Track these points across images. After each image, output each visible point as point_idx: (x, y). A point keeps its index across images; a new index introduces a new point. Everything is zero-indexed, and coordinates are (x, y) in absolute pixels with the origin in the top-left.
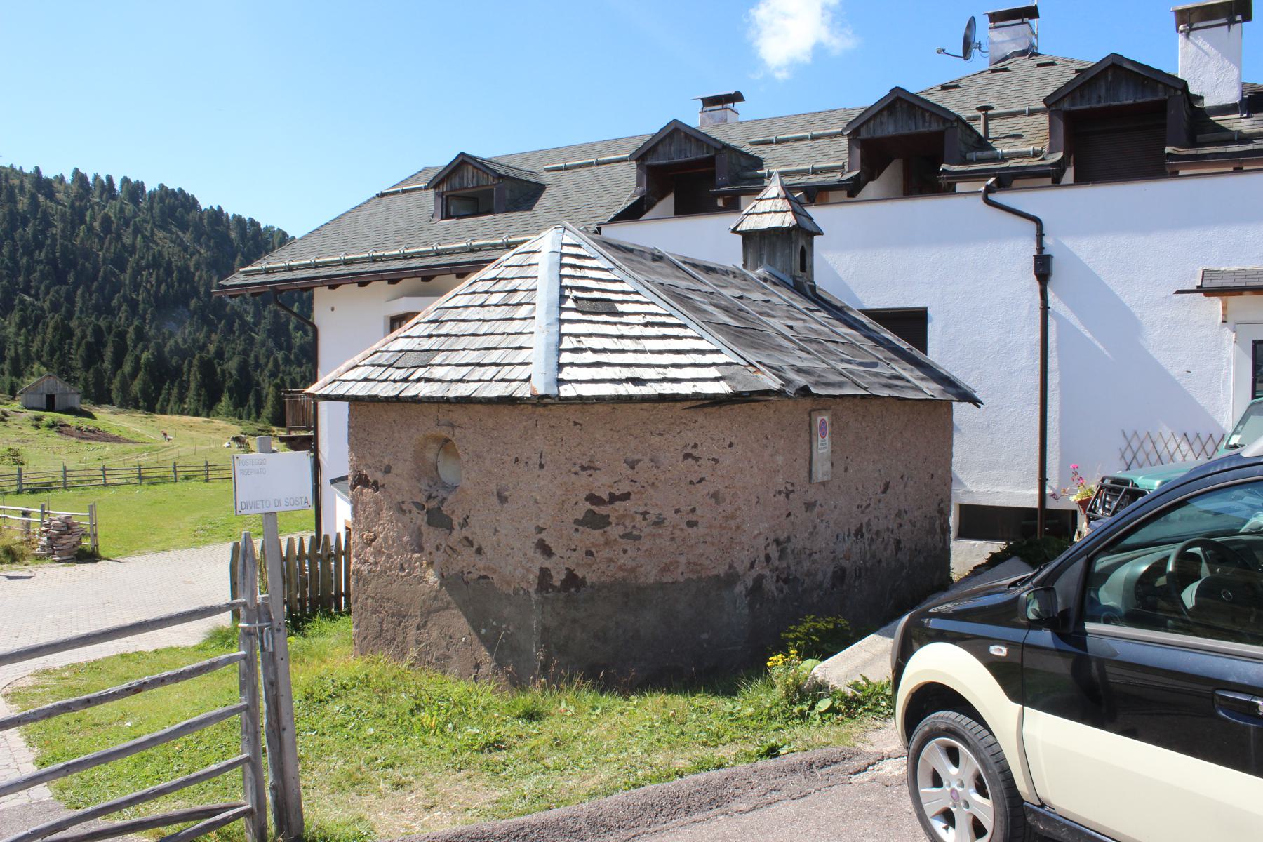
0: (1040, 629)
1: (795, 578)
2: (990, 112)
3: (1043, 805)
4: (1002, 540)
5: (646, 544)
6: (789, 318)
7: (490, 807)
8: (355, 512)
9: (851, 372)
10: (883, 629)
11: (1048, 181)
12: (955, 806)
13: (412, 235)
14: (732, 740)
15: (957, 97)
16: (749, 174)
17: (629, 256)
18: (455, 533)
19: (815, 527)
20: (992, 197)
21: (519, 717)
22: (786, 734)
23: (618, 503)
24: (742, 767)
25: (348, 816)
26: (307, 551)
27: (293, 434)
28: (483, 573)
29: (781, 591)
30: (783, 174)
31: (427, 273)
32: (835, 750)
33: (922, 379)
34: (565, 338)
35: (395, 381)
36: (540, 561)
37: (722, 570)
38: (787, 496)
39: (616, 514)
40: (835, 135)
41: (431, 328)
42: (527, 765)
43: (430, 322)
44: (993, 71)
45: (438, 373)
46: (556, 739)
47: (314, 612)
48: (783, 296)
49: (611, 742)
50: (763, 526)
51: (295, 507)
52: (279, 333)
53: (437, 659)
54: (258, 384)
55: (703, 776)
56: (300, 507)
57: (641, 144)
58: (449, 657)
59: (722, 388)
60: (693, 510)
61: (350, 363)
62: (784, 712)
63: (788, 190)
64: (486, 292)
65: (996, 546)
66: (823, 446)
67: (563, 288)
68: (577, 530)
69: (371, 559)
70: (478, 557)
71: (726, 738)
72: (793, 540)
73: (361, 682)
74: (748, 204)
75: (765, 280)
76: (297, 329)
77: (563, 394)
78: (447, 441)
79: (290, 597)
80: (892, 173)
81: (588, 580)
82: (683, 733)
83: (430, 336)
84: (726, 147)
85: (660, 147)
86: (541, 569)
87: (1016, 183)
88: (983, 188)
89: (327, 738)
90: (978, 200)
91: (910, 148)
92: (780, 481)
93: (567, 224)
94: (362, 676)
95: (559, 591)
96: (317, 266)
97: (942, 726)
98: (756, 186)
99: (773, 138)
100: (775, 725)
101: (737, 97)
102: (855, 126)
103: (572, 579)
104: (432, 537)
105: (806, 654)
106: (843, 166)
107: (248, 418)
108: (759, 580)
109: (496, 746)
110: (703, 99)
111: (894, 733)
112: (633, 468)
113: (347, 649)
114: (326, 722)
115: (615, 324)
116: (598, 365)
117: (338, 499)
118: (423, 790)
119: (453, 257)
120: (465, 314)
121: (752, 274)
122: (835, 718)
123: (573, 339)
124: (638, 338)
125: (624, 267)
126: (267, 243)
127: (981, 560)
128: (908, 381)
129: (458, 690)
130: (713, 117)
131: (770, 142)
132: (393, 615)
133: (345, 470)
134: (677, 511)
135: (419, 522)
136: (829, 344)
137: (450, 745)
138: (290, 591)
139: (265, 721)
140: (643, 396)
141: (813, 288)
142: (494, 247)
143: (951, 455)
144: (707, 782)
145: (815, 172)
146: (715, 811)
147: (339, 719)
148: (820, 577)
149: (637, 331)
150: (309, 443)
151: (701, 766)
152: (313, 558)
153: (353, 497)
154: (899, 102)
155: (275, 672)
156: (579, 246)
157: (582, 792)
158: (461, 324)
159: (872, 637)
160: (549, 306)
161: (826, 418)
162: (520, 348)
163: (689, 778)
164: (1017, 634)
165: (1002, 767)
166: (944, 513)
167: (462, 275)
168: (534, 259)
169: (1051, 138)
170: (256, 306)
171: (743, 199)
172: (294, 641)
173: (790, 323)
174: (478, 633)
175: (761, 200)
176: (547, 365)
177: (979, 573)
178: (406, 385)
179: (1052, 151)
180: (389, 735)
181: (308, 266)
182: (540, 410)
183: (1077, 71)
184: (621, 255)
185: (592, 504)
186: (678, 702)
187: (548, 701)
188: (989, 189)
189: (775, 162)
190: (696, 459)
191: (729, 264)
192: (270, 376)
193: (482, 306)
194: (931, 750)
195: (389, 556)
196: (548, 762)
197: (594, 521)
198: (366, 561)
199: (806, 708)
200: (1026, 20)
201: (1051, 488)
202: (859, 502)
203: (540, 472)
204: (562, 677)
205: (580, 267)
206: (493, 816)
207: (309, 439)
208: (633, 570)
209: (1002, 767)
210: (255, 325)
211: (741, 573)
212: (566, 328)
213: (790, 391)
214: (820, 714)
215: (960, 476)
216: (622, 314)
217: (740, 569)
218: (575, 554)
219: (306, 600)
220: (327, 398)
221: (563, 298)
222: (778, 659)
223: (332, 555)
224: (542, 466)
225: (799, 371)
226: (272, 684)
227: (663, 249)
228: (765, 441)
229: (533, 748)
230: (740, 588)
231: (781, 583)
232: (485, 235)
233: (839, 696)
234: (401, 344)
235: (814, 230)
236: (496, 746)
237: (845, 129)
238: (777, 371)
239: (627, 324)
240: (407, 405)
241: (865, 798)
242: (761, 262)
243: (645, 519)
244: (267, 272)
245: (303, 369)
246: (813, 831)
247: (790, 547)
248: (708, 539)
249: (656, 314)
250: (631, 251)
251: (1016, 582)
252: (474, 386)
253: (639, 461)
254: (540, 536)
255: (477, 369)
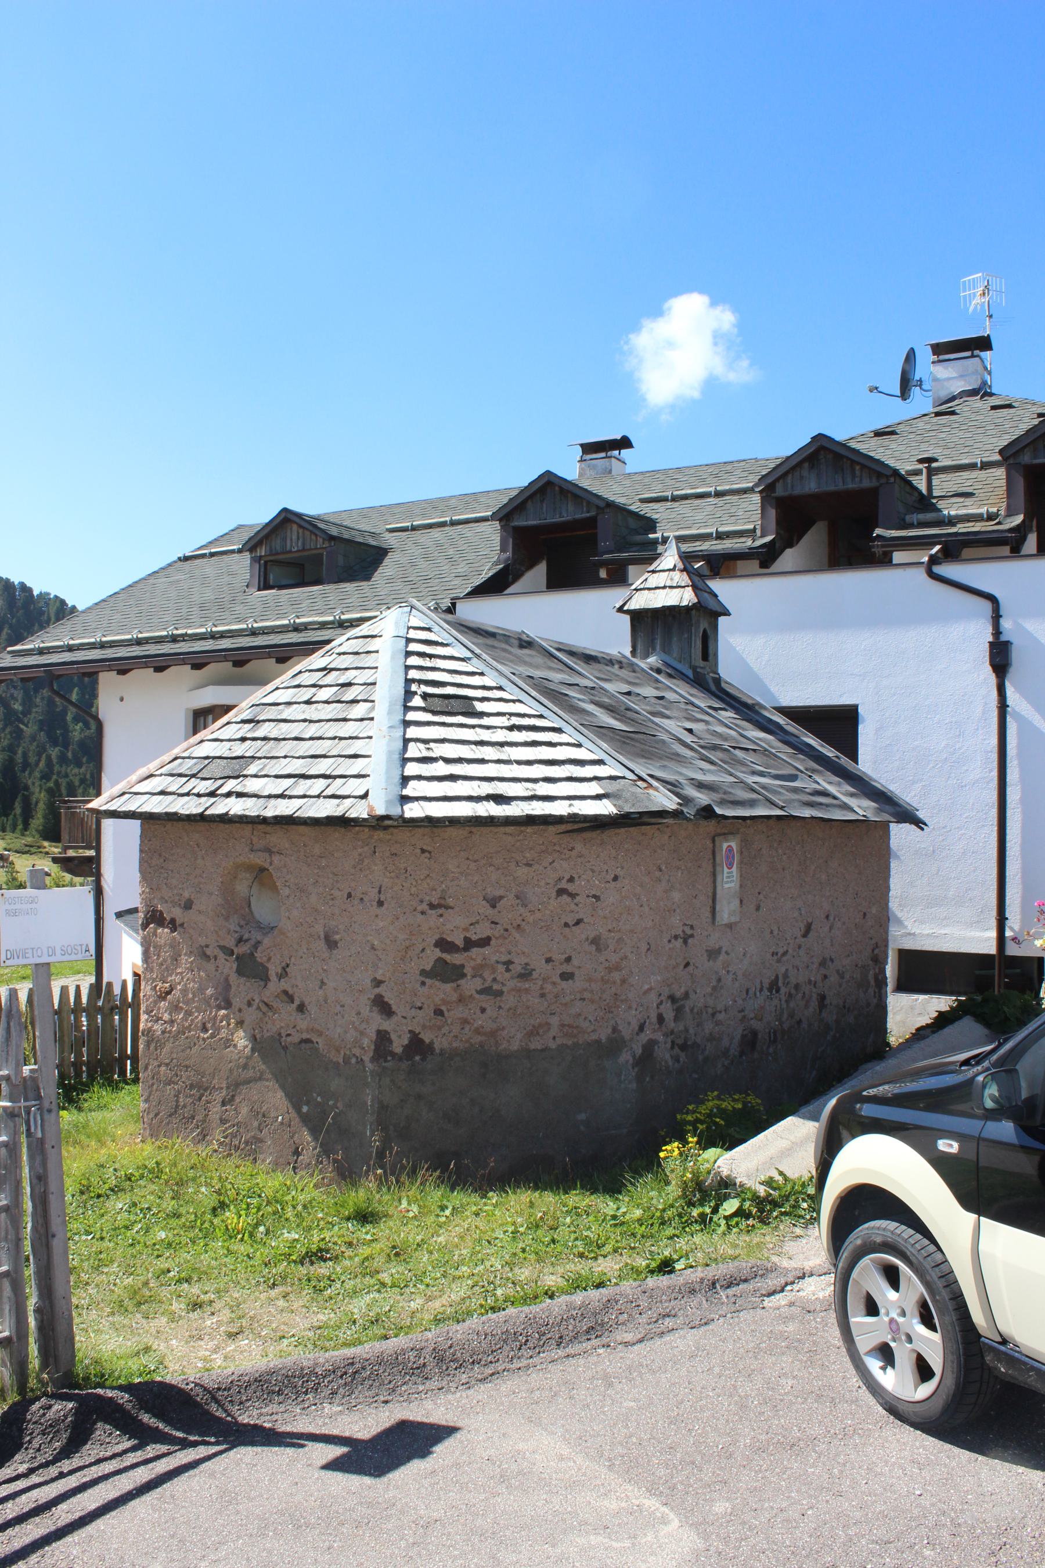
0: (1000, 1120)
1: (695, 1043)
2: (934, 465)
3: (1004, 1342)
4: (951, 994)
5: (509, 1000)
6: (688, 719)
7: (311, 1334)
8: (146, 956)
9: (764, 787)
10: (804, 1110)
11: (1006, 550)
12: (894, 1340)
13: (222, 608)
14: (615, 1251)
15: (893, 446)
16: (639, 538)
17: (490, 641)
18: (271, 985)
19: (719, 980)
20: (938, 569)
21: (348, 1219)
22: (682, 1243)
23: (475, 950)
24: (628, 1286)
25: (131, 1344)
26: (84, 1000)
27: (71, 853)
28: (305, 1036)
29: (677, 1059)
30: (680, 539)
31: (241, 656)
32: (745, 1265)
33: (852, 795)
34: (411, 745)
35: (199, 795)
36: (378, 1022)
37: (603, 1034)
38: (685, 942)
39: (472, 963)
40: (745, 491)
41: (245, 730)
42: (358, 1280)
43: (244, 722)
44: (937, 414)
45: (252, 785)
46: (394, 1247)
47: (92, 1078)
48: (679, 691)
49: (464, 1252)
50: (655, 979)
51: (73, 957)
52: (54, 725)
53: (247, 1143)
54: (26, 788)
55: (578, 1298)
56: (79, 957)
57: (505, 501)
58: (261, 1141)
59: (606, 808)
60: (568, 960)
61: (143, 771)
62: (680, 1216)
63: (687, 558)
64: (314, 686)
65: (943, 1003)
66: (729, 879)
67: (408, 682)
68: (423, 983)
69: (166, 1017)
70: (300, 1016)
71: (608, 1248)
72: (692, 996)
73: (151, 1172)
74: (638, 577)
75: (659, 671)
76: (76, 719)
77: (408, 814)
78: (263, 870)
79: (62, 1060)
80: (815, 538)
81: (437, 1046)
82: (553, 1241)
83: (243, 739)
84: (610, 505)
85: (529, 504)
86: (379, 1032)
87: (966, 552)
88: (926, 559)
89: (107, 1244)
90: (921, 574)
91: (836, 509)
92: (676, 923)
93: (415, 602)
94: (151, 1164)
95: (401, 1059)
96: (103, 645)
97: (879, 1240)
98: (648, 554)
99: (669, 494)
100: (670, 1231)
101: (624, 443)
102: (770, 480)
103: (417, 1045)
104: (242, 989)
105: (706, 1143)
106: (755, 529)
107: (13, 832)
108: (649, 1048)
109: (318, 1255)
110: (582, 445)
111: (818, 1244)
112: (494, 906)
113: (132, 1128)
114: (105, 1223)
115: (473, 727)
116: (453, 778)
117: (125, 937)
118: (226, 1311)
119: (272, 636)
120: (288, 713)
121: (642, 664)
122: (743, 1224)
123: (421, 746)
124: (502, 744)
125: (485, 656)
126: (42, 613)
127: (925, 1020)
128: (835, 798)
129: (272, 1183)
130: (594, 467)
131: (664, 499)
132: (192, 1087)
133: (134, 901)
134: (549, 960)
135: (226, 971)
136: (737, 752)
137: (261, 1254)
138: (62, 1052)
139: (29, 1225)
140: (507, 818)
141: (718, 681)
142: (323, 625)
143: (888, 889)
144: (584, 1306)
145: (720, 536)
146: (595, 1342)
147: (122, 1218)
148: (725, 1042)
149: (501, 736)
150: (87, 868)
151: (577, 1285)
152: (92, 1010)
153: (144, 938)
154: (822, 452)
155: (44, 1164)
156: (429, 629)
157: (427, 1317)
158: (282, 725)
159: (790, 1120)
160: (392, 704)
161: (733, 844)
162: (355, 756)
163: (562, 1300)
164: (971, 1126)
165: (953, 1292)
166: (879, 961)
167: (282, 660)
168: (374, 645)
169: (1008, 497)
170: (26, 692)
171: (632, 569)
172: (67, 1117)
173: (689, 725)
174: (298, 1110)
175: (653, 572)
176: (388, 778)
177: (924, 1038)
178: (213, 800)
179: (1010, 513)
180: (184, 1240)
181: (92, 646)
182: (380, 834)
183: (1040, 415)
184: (481, 640)
185: (442, 951)
186: (548, 1201)
187: (386, 1198)
188: (933, 560)
189: (671, 523)
190: (573, 896)
191: (613, 651)
192: (42, 778)
193: (308, 702)
194: (866, 1266)
195: (189, 1013)
196: (385, 1277)
197: (445, 972)
198: (159, 1019)
199: (708, 1210)
200: (976, 352)
201: (1012, 929)
202: (773, 949)
203: (379, 911)
204: (403, 1168)
205: (431, 656)
206: (315, 1345)
207: (90, 859)
208: (493, 1034)
209: (953, 1292)
210: (25, 713)
211: (627, 1037)
212: (412, 732)
213: (689, 811)
214: (726, 1218)
215: (899, 915)
216: (482, 715)
217: (626, 1032)
218: (421, 1013)
219: (82, 1063)
220: (114, 814)
221: (409, 694)
222: (673, 1148)
223: (117, 1007)
224: (380, 903)
225: (701, 786)
226: (40, 1179)
227: (533, 632)
228: (658, 874)
229: (367, 1259)
230: (625, 1057)
231: (677, 1050)
232: (311, 611)
233: (749, 1195)
234: (208, 749)
235: (719, 609)
236: (318, 1255)
237: (757, 485)
238: (673, 787)
239: (488, 728)
240: (213, 825)
241: (782, 1327)
242: (654, 649)
243: (508, 970)
244: (41, 652)
245: (83, 770)
246: (717, 1370)
247: (688, 1004)
248: (587, 995)
249: (523, 716)
250: (493, 635)
251: (968, 1049)
252: (297, 803)
253: (501, 898)
254: (377, 991)
255: (302, 781)
